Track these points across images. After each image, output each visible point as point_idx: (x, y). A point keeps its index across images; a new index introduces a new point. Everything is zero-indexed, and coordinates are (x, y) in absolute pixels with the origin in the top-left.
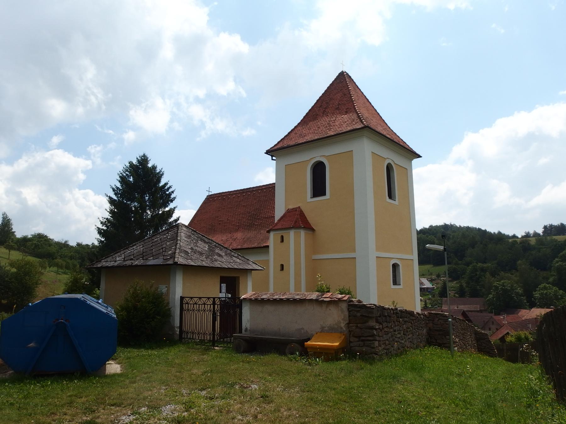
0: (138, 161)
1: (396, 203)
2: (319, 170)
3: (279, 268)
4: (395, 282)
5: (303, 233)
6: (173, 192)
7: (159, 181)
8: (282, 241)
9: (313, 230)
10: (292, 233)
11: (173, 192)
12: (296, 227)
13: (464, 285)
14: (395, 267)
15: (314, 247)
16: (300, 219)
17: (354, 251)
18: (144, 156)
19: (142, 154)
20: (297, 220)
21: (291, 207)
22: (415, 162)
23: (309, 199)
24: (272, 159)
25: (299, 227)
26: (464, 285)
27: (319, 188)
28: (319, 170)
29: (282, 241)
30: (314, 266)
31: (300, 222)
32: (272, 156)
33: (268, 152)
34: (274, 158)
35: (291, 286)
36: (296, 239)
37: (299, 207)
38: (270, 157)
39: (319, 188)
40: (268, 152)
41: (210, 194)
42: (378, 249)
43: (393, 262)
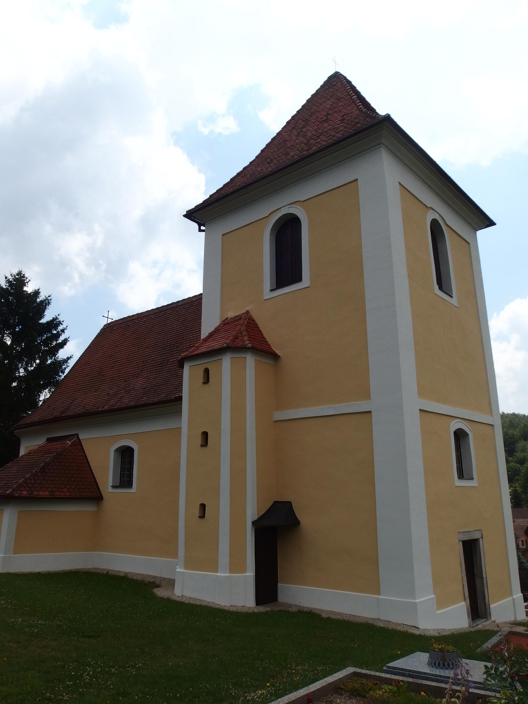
0: (8, 281)
1: (454, 301)
2: (287, 232)
3: (199, 441)
4: (461, 475)
5: (250, 361)
6: (63, 331)
7: (41, 315)
8: (207, 380)
9: (275, 357)
10: (226, 361)
11: (63, 331)
12: (234, 348)
13: (519, 489)
14: (460, 436)
15: (278, 391)
16: (245, 333)
17: (366, 395)
18: (19, 273)
19: (15, 272)
20: (245, 337)
21: (231, 314)
22: (483, 235)
23: (267, 294)
24: (200, 230)
25: (242, 349)
26: (519, 489)
27: (287, 270)
28: (287, 232)
29: (207, 380)
30: (278, 438)
31: (246, 338)
32: (200, 225)
33: (190, 215)
34: (203, 228)
35: (222, 481)
36: (236, 377)
37: (248, 312)
38: (196, 226)
39: (287, 270)
40: (190, 215)
41: (110, 321)
42: (422, 393)
43: (455, 425)
